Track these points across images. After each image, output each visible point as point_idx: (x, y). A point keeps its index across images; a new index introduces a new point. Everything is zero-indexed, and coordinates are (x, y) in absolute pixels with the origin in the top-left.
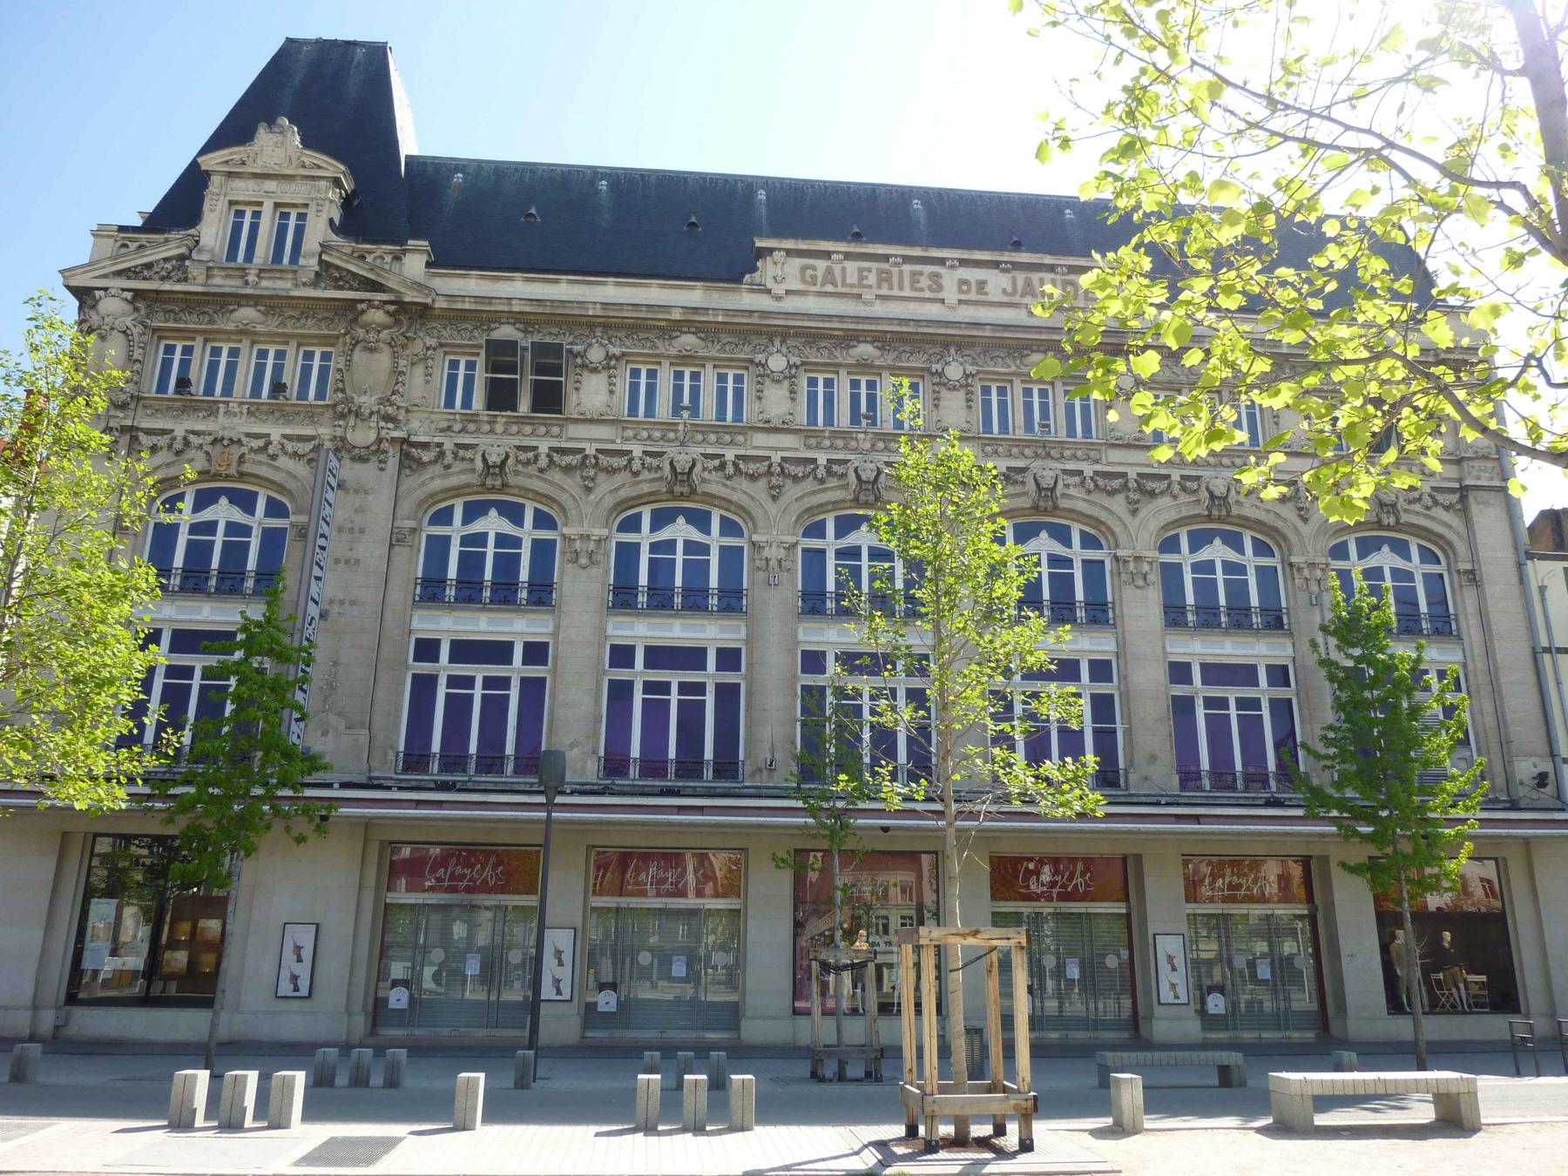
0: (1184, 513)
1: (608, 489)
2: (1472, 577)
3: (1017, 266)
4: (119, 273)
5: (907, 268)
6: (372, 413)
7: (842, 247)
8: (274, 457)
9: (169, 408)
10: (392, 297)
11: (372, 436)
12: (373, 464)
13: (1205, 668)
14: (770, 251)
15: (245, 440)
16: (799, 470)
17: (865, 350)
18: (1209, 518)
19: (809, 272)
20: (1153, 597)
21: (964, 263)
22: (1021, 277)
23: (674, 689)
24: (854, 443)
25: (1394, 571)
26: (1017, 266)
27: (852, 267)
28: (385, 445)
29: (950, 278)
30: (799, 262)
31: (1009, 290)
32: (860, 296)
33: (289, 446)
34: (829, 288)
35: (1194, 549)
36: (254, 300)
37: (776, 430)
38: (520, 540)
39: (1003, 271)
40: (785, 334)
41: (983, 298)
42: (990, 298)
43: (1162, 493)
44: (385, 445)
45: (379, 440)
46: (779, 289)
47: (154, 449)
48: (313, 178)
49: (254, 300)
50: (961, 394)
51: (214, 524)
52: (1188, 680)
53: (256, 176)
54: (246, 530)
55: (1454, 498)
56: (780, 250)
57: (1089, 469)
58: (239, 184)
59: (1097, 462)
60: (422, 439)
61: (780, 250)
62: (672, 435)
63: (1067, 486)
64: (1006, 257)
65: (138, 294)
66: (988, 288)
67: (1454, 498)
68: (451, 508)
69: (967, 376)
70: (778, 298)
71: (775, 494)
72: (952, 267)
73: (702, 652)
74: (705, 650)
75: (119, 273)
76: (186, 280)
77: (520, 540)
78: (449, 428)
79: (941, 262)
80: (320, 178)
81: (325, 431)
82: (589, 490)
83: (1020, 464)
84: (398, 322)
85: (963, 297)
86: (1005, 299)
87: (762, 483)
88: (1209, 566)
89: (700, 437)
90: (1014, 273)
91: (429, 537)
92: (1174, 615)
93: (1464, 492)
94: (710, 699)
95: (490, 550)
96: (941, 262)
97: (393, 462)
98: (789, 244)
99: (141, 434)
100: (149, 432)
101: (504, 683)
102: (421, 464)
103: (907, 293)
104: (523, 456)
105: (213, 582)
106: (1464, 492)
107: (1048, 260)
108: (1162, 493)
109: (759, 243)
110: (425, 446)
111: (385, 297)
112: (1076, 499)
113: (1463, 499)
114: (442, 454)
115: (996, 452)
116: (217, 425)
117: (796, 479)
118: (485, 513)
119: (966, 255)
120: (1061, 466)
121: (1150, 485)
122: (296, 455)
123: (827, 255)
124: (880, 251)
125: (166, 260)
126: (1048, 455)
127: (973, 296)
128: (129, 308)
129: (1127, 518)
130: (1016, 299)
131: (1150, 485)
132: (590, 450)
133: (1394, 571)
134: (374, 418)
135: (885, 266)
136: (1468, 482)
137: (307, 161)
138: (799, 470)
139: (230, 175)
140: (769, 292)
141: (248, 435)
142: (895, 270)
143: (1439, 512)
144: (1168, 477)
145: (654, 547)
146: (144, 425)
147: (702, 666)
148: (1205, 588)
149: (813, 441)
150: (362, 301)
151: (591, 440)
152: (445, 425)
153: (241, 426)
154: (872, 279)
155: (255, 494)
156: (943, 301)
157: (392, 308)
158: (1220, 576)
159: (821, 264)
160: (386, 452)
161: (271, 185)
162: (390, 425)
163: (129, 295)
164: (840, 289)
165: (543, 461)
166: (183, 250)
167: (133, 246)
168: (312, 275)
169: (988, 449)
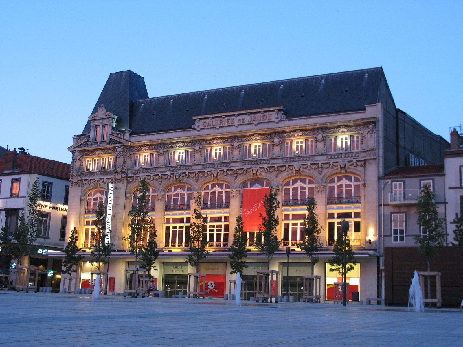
0: (289, 175)
1: (240, 179)
3: (251, 113)
5: (226, 118)
6: (120, 172)
7: (211, 116)
9: (88, 175)
11: (121, 177)
12: (121, 183)
14: (196, 120)
15: (100, 180)
18: (341, 173)
19: (205, 123)
21: (239, 115)
22: (253, 116)
23: (299, 224)
24: (214, 166)
26: (251, 113)
27: (214, 120)
28: (123, 179)
29: (236, 119)
31: (250, 120)
32: (216, 127)
34: (209, 127)
36: (100, 149)
37: (197, 165)
38: (351, 185)
39: (248, 115)
41: (244, 123)
42: (246, 123)
43: (284, 171)
44: (123, 179)
46: (198, 129)
47: (86, 184)
49: (100, 149)
50: (238, 150)
51: (342, 185)
52: (355, 217)
53: (99, 119)
54: (305, 188)
56: (198, 119)
57: (266, 166)
58: (96, 122)
59: (269, 163)
60: (130, 176)
61: (198, 119)
62: (176, 169)
63: (261, 171)
64: (249, 111)
66: (245, 120)
68: (289, 181)
69: (239, 145)
70: (198, 131)
71: (320, 173)
72: (236, 116)
74: (170, 219)
75: (77, 147)
77: (306, 188)
78: (135, 173)
79: (233, 115)
80: (110, 118)
81: (112, 176)
82: (160, 184)
83: (249, 167)
85: (239, 124)
86: (249, 123)
89: (182, 168)
90: (251, 115)
91: (329, 186)
95: (299, 191)
96: (233, 115)
97: (125, 181)
98: (200, 117)
99: (83, 181)
100: (85, 180)
102: (130, 182)
103: (226, 125)
104: (304, 167)
105: (216, 206)
107: (258, 110)
108: (284, 171)
109: (193, 118)
111: (121, 145)
112: (351, 169)
113: (365, 163)
115: (245, 164)
118: (342, 179)
119: (214, 116)
120: (259, 166)
123: (208, 118)
124: (219, 115)
125: (85, 142)
126: (257, 163)
127: (241, 123)
128: (123, 150)
130: (251, 122)
132: (235, 169)
134: (121, 173)
135: (221, 119)
137: (107, 114)
140: (196, 130)
141: (101, 179)
142: (224, 119)
144: (285, 166)
145: (293, 189)
146: (84, 179)
148: (340, 193)
150: (117, 146)
151: (160, 172)
152: (134, 172)
154: (219, 123)
155: (223, 184)
156: (234, 125)
157: (122, 147)
159: (207, 121)
160: (123, 180)
161: (101, 121)
162: (124, 174)
164: (211, 127)
165: (355, 165)
166: (87, 140)
167: (80, 139)
168: (108, 142)
169: (243, 163)
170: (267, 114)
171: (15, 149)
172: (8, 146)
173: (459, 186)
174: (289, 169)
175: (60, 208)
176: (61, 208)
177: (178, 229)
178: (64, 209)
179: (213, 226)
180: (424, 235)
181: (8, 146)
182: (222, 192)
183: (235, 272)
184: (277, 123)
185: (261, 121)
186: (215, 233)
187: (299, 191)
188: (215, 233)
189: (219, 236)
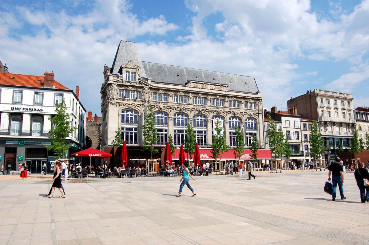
2: (259, 123)
4: (115, 81)
8: (136, 107)
10: (148, 86)
13: (233, 133)
16: (193, 110)
17: (200, 95)
20: (228, 125)
22: (216, 86)
25: (235, 121)
27: (198, 84)
30: (193, 83)
33: (138, 105)
35: (126, 112)
40: (191, 93)
45: (116, 103)
46: (191, 87)
48: (136, 69)
52: (231, 134)
55: (258, 114)
65: (118, 85)
67: (258, 114)
70: (217, 91)
73: (163, 130)
76: (123, 83)
84: (149, 90)
87: (189, 111)
88: (128, 115)
92: (175, 124)
93: (259, 114)
94: (164, 135)
101: (132, 133)
106: (259, 114)
110: (152, 106)
113: (258, 115)
114: (155, 107)
116: (128, 102)
117: (193, 111)
121: (229, 112)
122: (138, 106)
127: (211, 89)
129: (190, 113)
131: (229, 112)
133: (235, 121)
136: (259, 113)
138: (193, 110)
139: (126, 68)
143: (256, 116)
147: (163, 132)
149: (194, 106)
153: (132, 102)
158: (160, 118)
159: (195, 84)
161: (131, 69)
163: (116, 85)
170: (222, 87)
171: (314, 90)
172: (5, 64)
173: (294, 127)
174: (167, 108)
175: (33, 109)
176: (34, 109)
177: (129, 134)
178: (37, 110)
179: (199, 136)
180: (164, 144)
181: (5, 64)
184: (226, 92)
185: (220, 90)
186: (200, 139)
187: (200, 121)
188: (200, 139)
189: (202, 140)
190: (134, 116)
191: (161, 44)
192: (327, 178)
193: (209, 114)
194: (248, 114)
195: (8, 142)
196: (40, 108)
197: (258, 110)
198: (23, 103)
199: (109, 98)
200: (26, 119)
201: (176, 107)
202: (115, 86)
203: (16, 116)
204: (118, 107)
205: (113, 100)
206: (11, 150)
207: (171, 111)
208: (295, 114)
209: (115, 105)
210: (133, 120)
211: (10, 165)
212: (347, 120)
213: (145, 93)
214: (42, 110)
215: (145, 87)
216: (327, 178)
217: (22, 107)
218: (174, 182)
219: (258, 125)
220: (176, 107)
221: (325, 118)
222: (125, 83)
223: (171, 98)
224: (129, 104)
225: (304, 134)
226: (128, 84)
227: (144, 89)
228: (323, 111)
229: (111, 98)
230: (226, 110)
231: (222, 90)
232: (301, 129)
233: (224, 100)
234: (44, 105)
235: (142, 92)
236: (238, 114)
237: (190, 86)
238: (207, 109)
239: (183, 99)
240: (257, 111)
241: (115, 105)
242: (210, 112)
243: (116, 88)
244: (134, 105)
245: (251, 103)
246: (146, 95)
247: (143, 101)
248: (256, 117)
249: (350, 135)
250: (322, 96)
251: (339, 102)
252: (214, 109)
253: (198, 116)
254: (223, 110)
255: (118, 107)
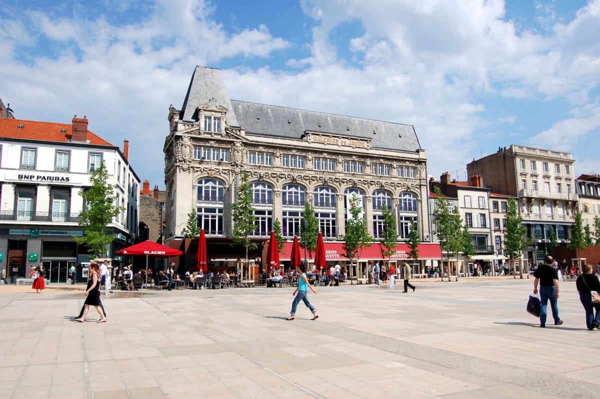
2: (421, 201)
4: (187, 133)
8: (220, 174)
10: (241, 141)
13: (379, 216)
16: (314, 178)
17: (325, 155)
20: (371, 203)
22: (352, 140)
25: (383, 198)
27: (323, 137)
30: (313, 136)
33: (224, 171)
35: (205, 183)
40: (311, 151)
45: (189, 167)
46: (310, 141)
47: (197, 171)
48: (221, 112)
52: (376, 219)
55: (419, 186)
65: (191, 138)
67: (419, 186)
70: (353, 148)
73: (265, 212)
76: (200, 134)
84: (242, 146)
87: (308, 181)
88: (208, 187)
92: (284, 202)
93: (420, 185)
94: (267, 220)
101: (215, 217)
106: (420, 185)
110: (248, 172)
113: (420, 187)
114: (251, 174)
116: (209, 166)
117: (314, 180)
121: (372, 183)
122: (225, 173)
127: (343, 145)
129: (309, 185)
131: (372, 183)
133: (383, 198)
136: (422, 184)
138: (314, 178)
139: (204, 110)
143: (416, 189)
147: (265, 214)
149: (316, 173)
153: (214, 167)
158: (260, 193)
159: (317, 136)
161: (213, 113)
163: (189, 138)
170: (361, 142)
171: (511, 146)
172: (9, 104)
173: (478, 208)
174: (271, 176)
177: (210, 218)
179: (323, 221)
180: (267, 235)
181: (9, 104)
182: (264, 191)
183: (416, 251)
184: (368, 150)
185: (358, 146)
186: (325, 226)
187: (325, 196)
188: (325, 226)
189: (328, 229)
190: (217, 189)
191: (262, 71)
192: (531, 290)
193: (340, 186)
194: (404, 186)
195: (12, 232)
196: (65, 175)
197: (420, 180)
198: (38, 168)
199: (178, 160)
200: (43, 193)
201: (286, 174)
202: (186, 141)
203: (25, 189)
204: (191, 174)
205: (183, 162)
206: (18, 245)
207: (278, 182)
208: (480, 186)
209: (188, 171)
210: (216, 195)
211: (16, 269)
212: (564, 196)
213: (235, 151)
214: (68, 179)
215: (235, 142)
216: (531, 290)
217: (36, 174)
218: (283, 296)
219: (420, 204)
220: (286, 174)
221: (529, 192)
222: (203, 135)
223: (278, 160)
224: (209, 170)
225: (495, 219)
226: (209, 136)
227: (233, 145)
228: (524, 181)
229: (181, 159)
230: (367, 180)
231: (361, 147)
232: (489, 209)
233: (364, 162)
234: (71, 171)
235: (232, 150)
236: (387, 186)
237: (308, 140)
238: (337, 177)
239: (298, 161)
240: (418, 181)
241: (188, 171)
242: (341, 183)
243: (189, 143)
244: (217, 171)
245: (408, 167)
246: (238, 156)
247: (233, 164)
248: (417, 191)
249: (569, 219)
250: (524, 157)
251: (551, 166)
252: (348, 178)
253: (321, 189)
254: (362, 180)
255: (191, 174)
